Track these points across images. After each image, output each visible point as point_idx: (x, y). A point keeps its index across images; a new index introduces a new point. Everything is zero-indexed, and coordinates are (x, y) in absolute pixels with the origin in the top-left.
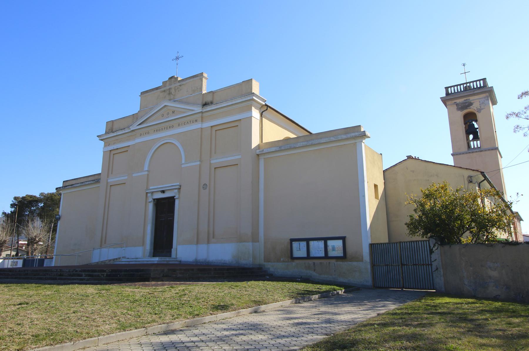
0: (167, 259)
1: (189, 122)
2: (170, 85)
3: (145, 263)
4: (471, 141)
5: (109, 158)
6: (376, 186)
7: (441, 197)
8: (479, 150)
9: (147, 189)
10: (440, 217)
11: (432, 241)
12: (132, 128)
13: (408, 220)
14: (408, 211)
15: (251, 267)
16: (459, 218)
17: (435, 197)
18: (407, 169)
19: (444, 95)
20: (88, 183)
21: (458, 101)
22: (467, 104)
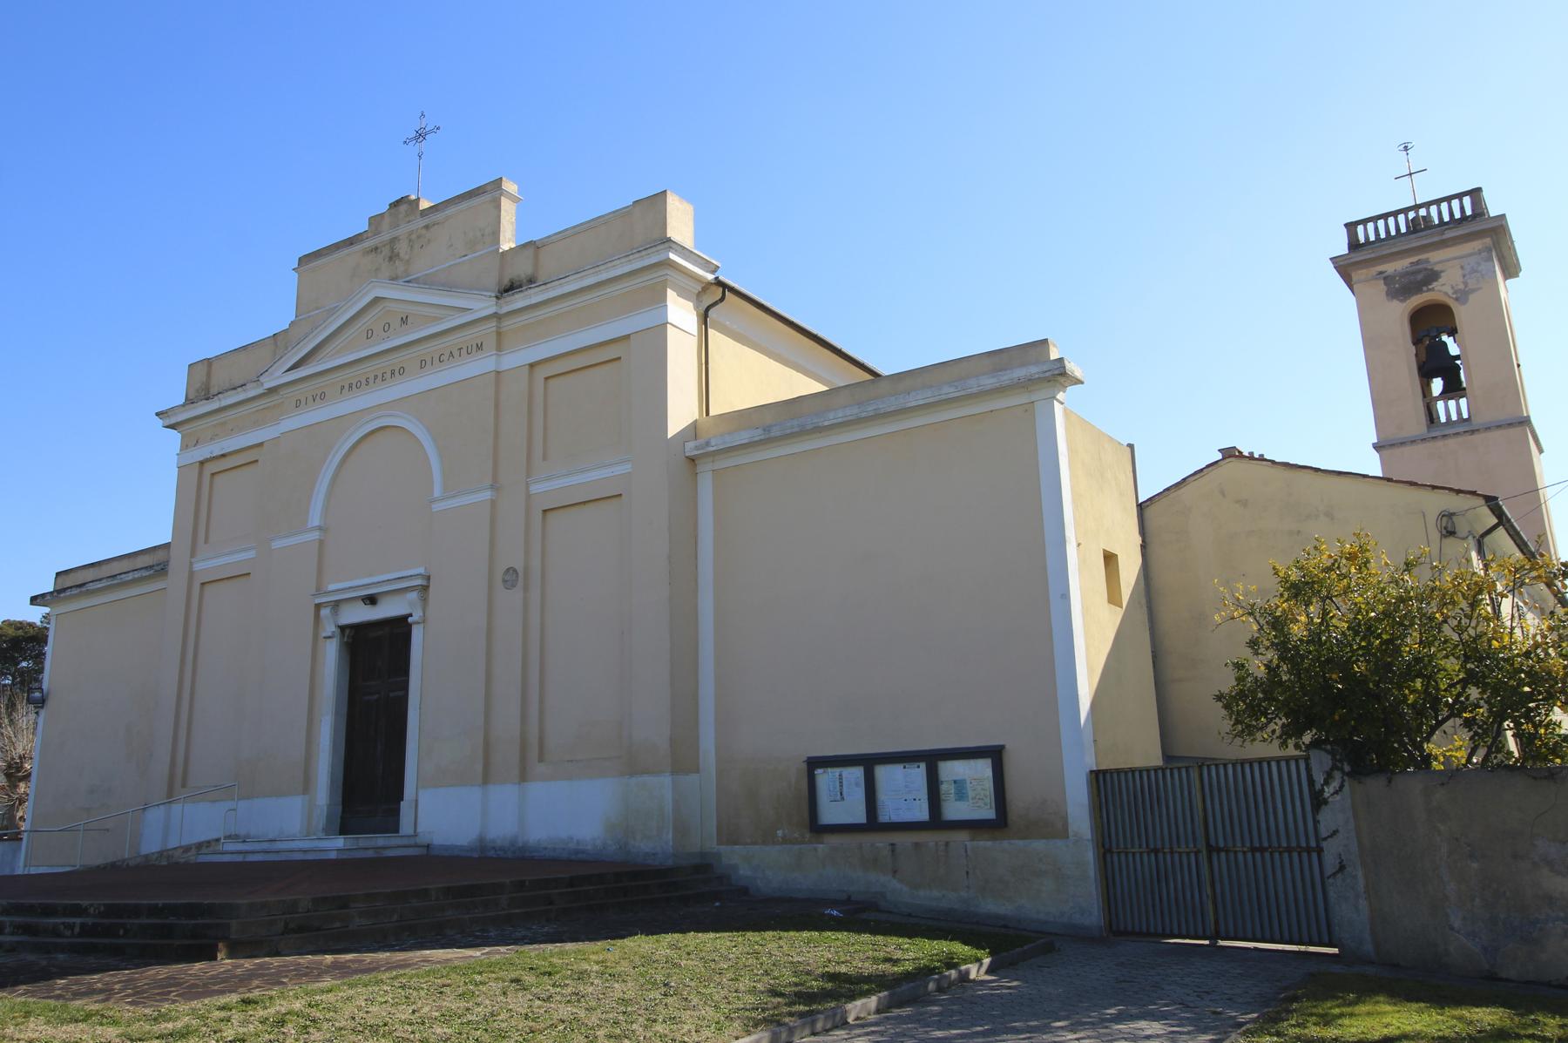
0: (380, 840)
1: (456, 353)
2: (395, 225)
3: (298, 857)
4: (1438, 399)
5: (200, 486)
6: (1110, 559)
7: (1347, 590)
8: (1464, 427)
9: (319, 591)
10: (1345, 667)
11: (1321, 762)
12: (269, 382)
13: (1228, 683)
14: (1227, 649)
15: (670, 863)
16: (1421, 667)
17: (1324, 593)
18: (1223, 493)
19: (1343, 249)
20: (130, 577)
21: (1391, 268)
22: (1420, 277)
